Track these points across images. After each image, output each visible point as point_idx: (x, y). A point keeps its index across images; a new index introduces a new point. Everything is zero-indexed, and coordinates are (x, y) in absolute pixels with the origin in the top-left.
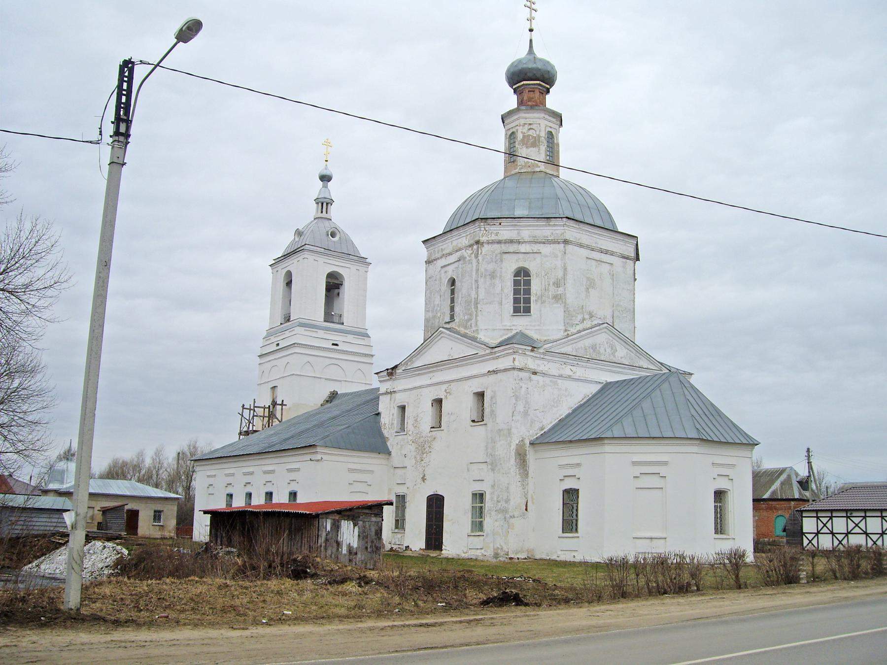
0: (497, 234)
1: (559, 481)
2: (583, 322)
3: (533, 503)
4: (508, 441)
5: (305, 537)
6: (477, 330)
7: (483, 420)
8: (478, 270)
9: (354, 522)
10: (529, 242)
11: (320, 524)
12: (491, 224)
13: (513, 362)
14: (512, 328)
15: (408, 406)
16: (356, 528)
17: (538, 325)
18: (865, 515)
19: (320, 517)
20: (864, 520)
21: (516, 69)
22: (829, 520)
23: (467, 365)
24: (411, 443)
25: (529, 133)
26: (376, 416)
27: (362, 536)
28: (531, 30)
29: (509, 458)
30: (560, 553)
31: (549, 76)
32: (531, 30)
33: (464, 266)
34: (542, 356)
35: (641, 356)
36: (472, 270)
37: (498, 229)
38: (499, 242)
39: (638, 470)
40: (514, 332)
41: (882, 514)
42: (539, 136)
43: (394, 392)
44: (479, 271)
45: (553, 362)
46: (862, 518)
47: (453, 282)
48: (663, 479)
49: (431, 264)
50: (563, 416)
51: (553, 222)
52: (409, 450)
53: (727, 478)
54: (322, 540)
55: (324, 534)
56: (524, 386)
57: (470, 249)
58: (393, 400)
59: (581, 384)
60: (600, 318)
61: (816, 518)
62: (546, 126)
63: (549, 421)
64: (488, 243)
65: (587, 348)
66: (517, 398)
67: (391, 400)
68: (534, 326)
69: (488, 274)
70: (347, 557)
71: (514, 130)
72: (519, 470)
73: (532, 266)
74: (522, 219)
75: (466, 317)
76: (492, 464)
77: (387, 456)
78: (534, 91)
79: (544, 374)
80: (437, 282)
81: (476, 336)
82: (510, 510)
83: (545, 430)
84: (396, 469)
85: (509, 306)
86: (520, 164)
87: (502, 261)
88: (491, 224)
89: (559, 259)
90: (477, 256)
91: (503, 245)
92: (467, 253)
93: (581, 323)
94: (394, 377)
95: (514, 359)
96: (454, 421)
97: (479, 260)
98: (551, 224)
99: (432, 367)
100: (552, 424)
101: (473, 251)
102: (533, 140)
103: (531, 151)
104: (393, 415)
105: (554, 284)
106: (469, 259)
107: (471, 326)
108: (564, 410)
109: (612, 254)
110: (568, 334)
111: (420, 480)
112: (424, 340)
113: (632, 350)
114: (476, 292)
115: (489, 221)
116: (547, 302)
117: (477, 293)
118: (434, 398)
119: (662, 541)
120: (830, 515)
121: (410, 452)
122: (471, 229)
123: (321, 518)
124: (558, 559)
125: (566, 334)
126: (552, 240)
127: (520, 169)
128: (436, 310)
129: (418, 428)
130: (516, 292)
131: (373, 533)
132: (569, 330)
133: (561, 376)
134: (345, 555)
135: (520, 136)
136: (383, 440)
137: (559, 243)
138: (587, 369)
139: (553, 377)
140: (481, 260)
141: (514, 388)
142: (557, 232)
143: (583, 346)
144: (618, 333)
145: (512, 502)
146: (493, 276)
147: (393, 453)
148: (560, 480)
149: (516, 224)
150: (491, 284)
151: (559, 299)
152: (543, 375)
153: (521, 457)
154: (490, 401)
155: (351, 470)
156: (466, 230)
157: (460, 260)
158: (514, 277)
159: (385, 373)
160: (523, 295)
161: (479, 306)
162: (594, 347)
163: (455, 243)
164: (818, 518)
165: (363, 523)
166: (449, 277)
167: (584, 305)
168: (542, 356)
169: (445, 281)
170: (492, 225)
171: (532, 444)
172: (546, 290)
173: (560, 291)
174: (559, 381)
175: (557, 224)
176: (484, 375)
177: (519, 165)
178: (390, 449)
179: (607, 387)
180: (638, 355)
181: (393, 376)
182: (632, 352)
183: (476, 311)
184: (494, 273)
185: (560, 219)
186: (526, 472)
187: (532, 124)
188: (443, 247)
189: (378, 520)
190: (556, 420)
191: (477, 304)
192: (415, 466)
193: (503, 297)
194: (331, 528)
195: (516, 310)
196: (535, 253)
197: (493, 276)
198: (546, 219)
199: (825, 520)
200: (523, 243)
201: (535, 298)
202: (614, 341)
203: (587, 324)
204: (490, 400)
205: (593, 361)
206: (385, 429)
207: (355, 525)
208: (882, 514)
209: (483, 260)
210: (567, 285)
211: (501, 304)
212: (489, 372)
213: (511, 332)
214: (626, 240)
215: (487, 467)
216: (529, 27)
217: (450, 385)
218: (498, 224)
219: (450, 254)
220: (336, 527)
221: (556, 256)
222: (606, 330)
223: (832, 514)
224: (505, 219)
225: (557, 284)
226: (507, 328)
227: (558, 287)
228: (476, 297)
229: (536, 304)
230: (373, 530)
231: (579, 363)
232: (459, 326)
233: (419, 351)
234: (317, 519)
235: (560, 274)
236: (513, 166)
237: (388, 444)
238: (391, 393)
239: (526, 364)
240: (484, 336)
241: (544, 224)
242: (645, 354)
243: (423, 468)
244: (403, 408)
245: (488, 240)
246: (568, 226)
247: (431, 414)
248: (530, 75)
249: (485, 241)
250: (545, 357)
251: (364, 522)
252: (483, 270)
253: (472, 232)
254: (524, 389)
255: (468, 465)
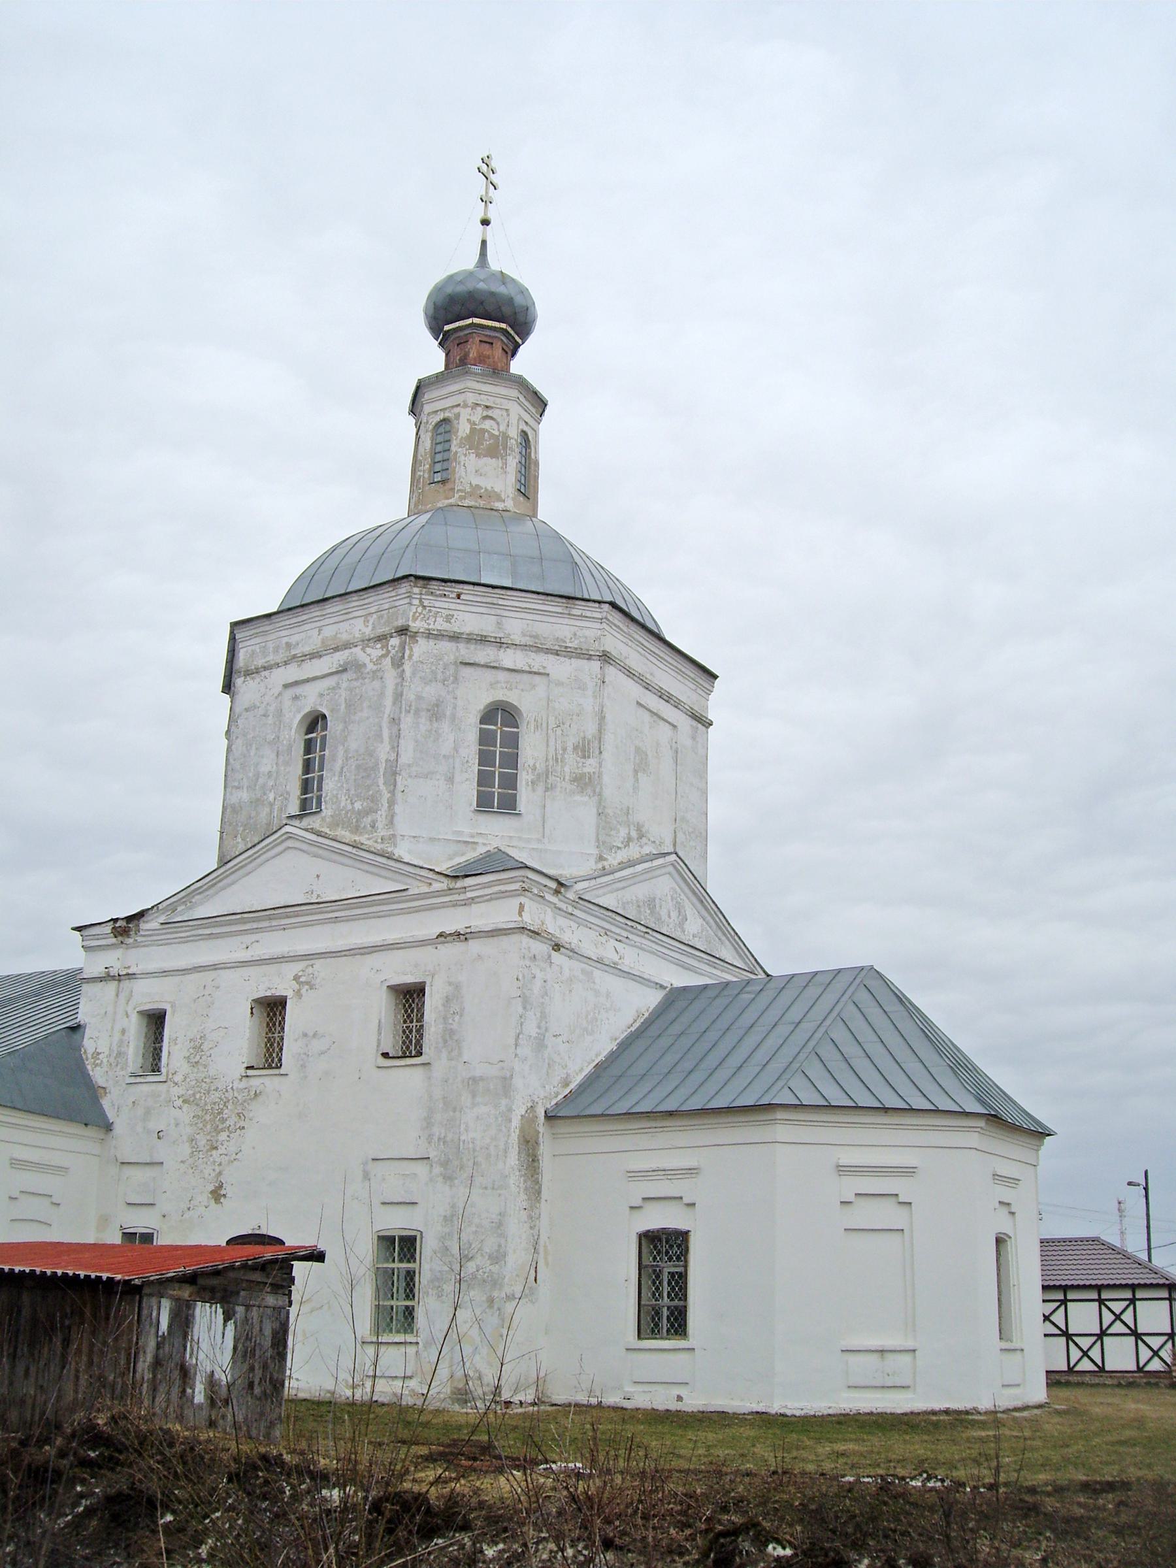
0: (448, 619)
1: (628, 1209)
2: (627, 845)
3: (547, 1264)
4: (503, 1108)
5: (79, 1351)
6: (394, 835)
7: (421, 1054)
8: (401, 695)
9: (226, 1306)
10: (524, 647)
11: (145, 1312)
12: (438, 592)
13: (521, 915)
14: (475, 840)
15: (174, 1012)
16: (231, 1326)
17: (539, 841)
18: (1134, 1295)
19: (146, 1290)
20: (1063, 1308)
21: (460, 289)
22: (1128, 1306)
23: (366, 917)
24: (179, 1102)
25: (483, 426)
26: (71, 1033)
27: (244, 1350)
28: (485, 222)
29: (506, 1151)
30: (630, 1389)
31: (526, 318)
32: (485, 222)
33: (355, 684)
34: (570, 909)
35: (724, 938)
36: (382, 695)
37: (453, 606)
38: (455, 637)
39: (851, 1186)
40: (482, 850)
41: (1099, 1295)
42: (506, 437)
43: (130, 976)
44: (404, 697)
45: (587, 926)
46: (1059, 1303)
47: (315, 722)
48: (905, 1209)
49: (253, 679)
50: (601, 1057)
51: (578, 609)
52: (173, 1121)
53: (893, 1199)
54: (144, 1364)
55: (152, 1344)
56: (540, 975)
57: (379, 646)
58: (123, 996)
59: (632, 984)
60: (654, 842)
61: (1097, 1304)
62: (520, 418)
63: (579, 1068)
64: (429, 635)
65: (641, 904)
66: (526, 1002)
67: (117, 995)
68: (528, 841)
69: (424, 706)
70: (205, 1413)
71: (447, 414)
72: (525, 1181)
73: (526, 700)
74: (509, 593)
75: (358, 806)
76: (445, 1164)
77: (101, 1134)
78: (492, 344)
79: (574, 953)
80: (270, 720)
81: (389, 850)
82: (506, 1280)
83: (572, 1086)
84: (125, 1167)
85: (468, 790)
86: (461, 488)
87: (456, 680)
88: (438, 592)
89: (589, 693)
90: (398, 663)
91: (462, 646)
92: (368, 656)
93: (625, 847)
94: (131, 941)
95: (522, 907)
96: (323, 1053)
97: (404, 670)
98: (574, 612)
99: (254, 920)
100: (584, 1074)
101: (388, 652)
102: (491, 441)
103: (486, 465)
104: (123, 1032)
105: (575, 748)
106: (375, 668)
107: (373, 827)
108: (604, 1046)
109: (677, 704)
110: (604, 868)
111: (204, 1198)
112: (221, 858)
113: (711, 921)
114: (393, 748)
115: (434, 586)
116: (559, 789)
117: (395, 748)
118: (261, 994)
119: (907, 1358)
120: (1063, 1298)
121: (177, 1125)
122: (382, 600)
123: (147, 1295)
124: (627, 1404)
125: (600, 866)
126: (576, 649)
127: (462, 498)
128: (264, 786)
129: (205, 1066)
130: (485, 758)
131: (268, 1342)
132: (606, 859)
133: (599, 961)
134: (200, 1406)
135: (463, 429)
136: (94, 1093)
137: (590, 657)
138: (641, 952)
139: (585, 960)
140: (408, 673)
141: (520, 978)
142: (587, 633)
143: (634, 898)
144: (693, 879)
145: (511, 1259)
146: (435, 712)
147: (118, 1129)
148: (632, 1208)
149: (495, 601)
150: (430, 731)
151: (585, 784)
152: (571, 954)
153: (529, 1146)
154: (441, 1008)
155: (17, 1164)
156: (366, 601)
157: (345, 670)
158: (481, 723)
159: (108, 929)
160: (500, 767)
161: (399, 778)
162: (651, 903)
163: (329, 632)
164: (1101, 1302)
165: (247, 1311)
166: (307, 710)
167: (631, 807)
168: (570, 909)
169: (295, 719)
170: (440, 596)
171: (550, 1117)
172: (557, 760)
173: (590, 765)
174: (597, 973)
175: (589, 614)
176: (423, 943)
177: (461, 491)
178: (111, 1115)
179: (675, 998)
180: (720, 934)
181: (129, 936)
182: (710, 927)
183: (393, 793)
184: (437, 706)
185: (597, 605)
186: (537, 1187)
187: (492, 408)
188: (294, 639)
189: (280, 1303)
190: (589, 1063)
191: (395, 774)
192: (191, 1160)
193: (457, 765)
194: (170, 1326)
195: (484, 803)
196: (535, 673)
197: (435, 712)
198: (564, 601)
199: (1117, 1307)
200: (509, 645)
201: (530, 777)
202: (683, 896)
203: (634, 852)
204: (444, 1005)
205: (655, 934)
206: (96, 1065)
207: (227, 1319)
208: (1099, 1295)
209: (414, 674)
210: (605, 755)
211: (450, 780)
212: (441, 935)
213: (475, 849)
214: (701, 682)
215: (431, 1172)
216: (480, 215)
217: (312, 966)
218: (454, 595)
219: (315, 655)
220: (183, 1321)
221: (582, 687)
222: (671, 869)
223: (1065, 1296)
224: (471, 587)
225: (583, 750)
226: (465, 839)
227: (584, 757)
228: (393, 756)
229: (534, 790)
230: (268, 1332)
231: (630, 936)
232: (335, 825)
233: (206, 885)
234: (138, 1297)
235: (591, 729)
236: (441, 490)
237: (106, 1103)
238: (119, 978)
239: (543, 924)
240: (410, 852)
241: (559, 610)
242: (733, 933)
243: (218, 1169)
244: (156, 1020)
245: (429, 630)
246: (611, 624)
247: (248, 1035)
248: (490, 308)
249: (421, 630)
250: (576, 912)
251: (248, 1307)
252: (413, 697)
253: (386, 606)
254: (538, 983)
255: (365, 1164)
